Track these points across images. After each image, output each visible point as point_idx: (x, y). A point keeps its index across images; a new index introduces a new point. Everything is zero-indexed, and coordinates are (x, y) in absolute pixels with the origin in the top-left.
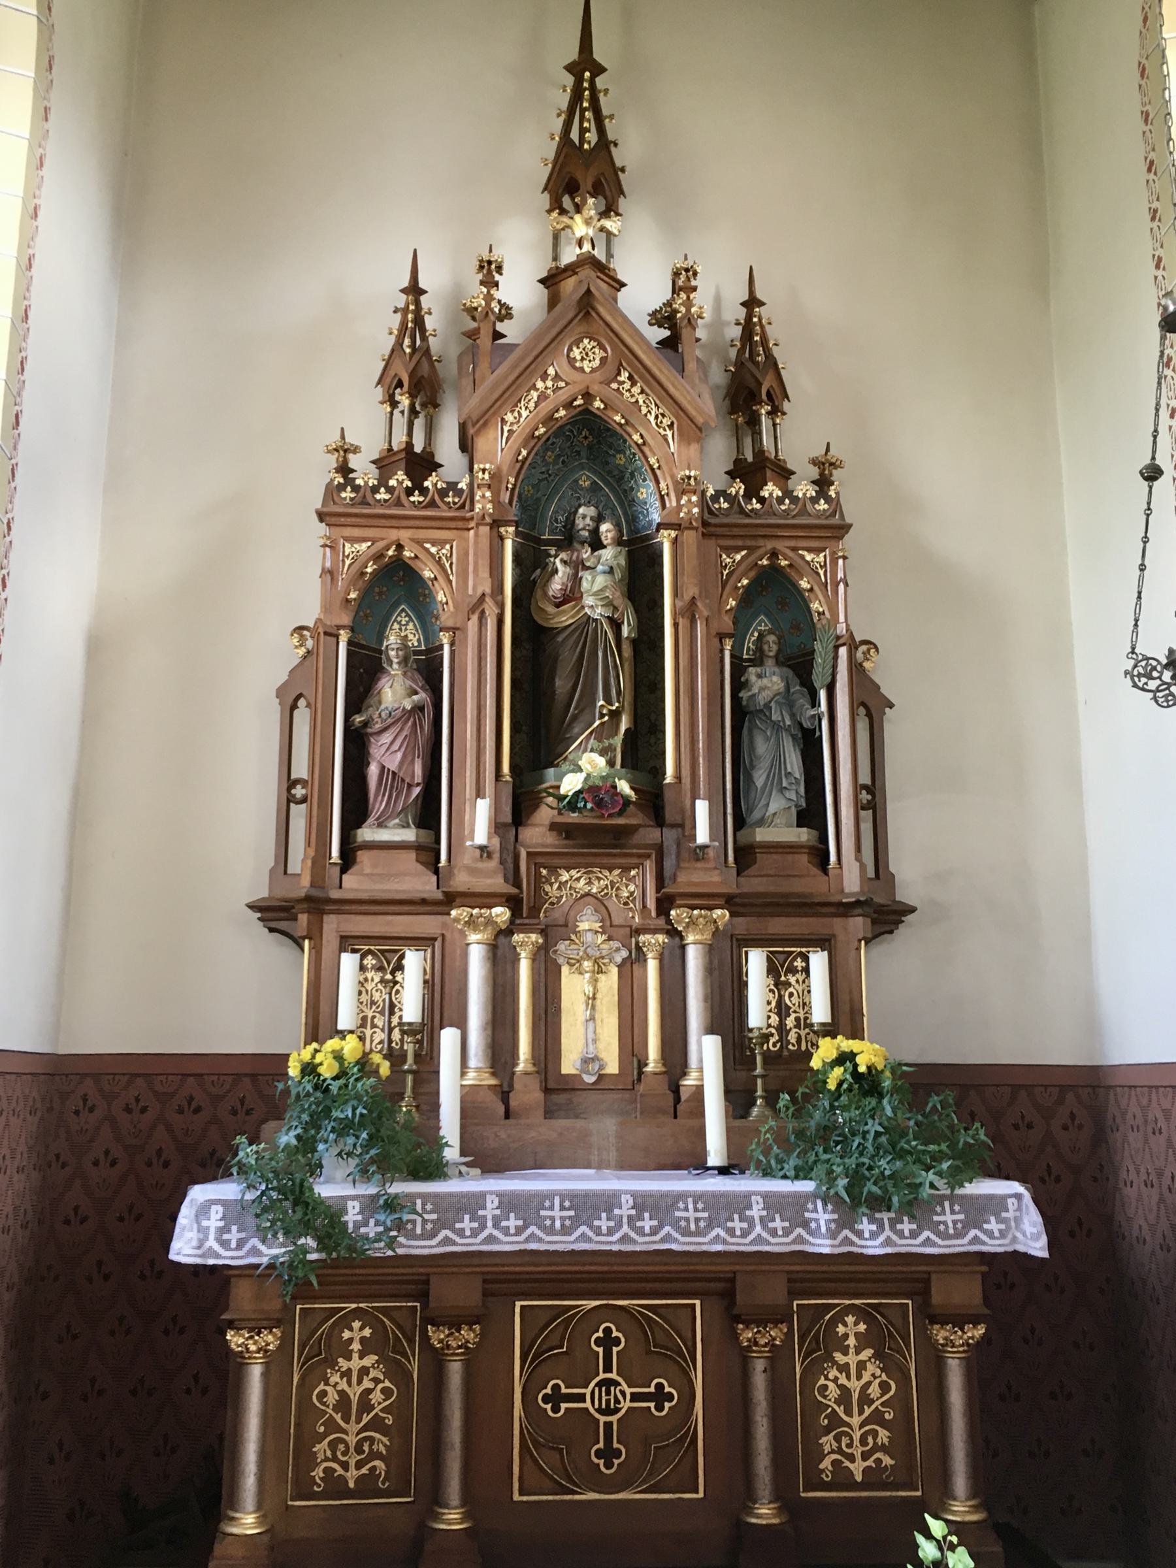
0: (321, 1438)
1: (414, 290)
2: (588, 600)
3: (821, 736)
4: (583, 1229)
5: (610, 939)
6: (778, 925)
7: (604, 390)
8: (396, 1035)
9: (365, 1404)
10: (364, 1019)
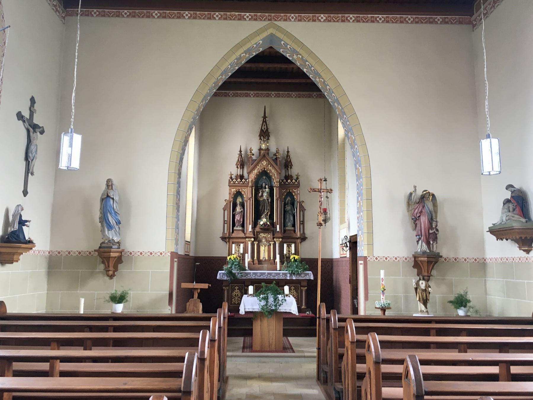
1: (241, 151)
9: (238, 295)
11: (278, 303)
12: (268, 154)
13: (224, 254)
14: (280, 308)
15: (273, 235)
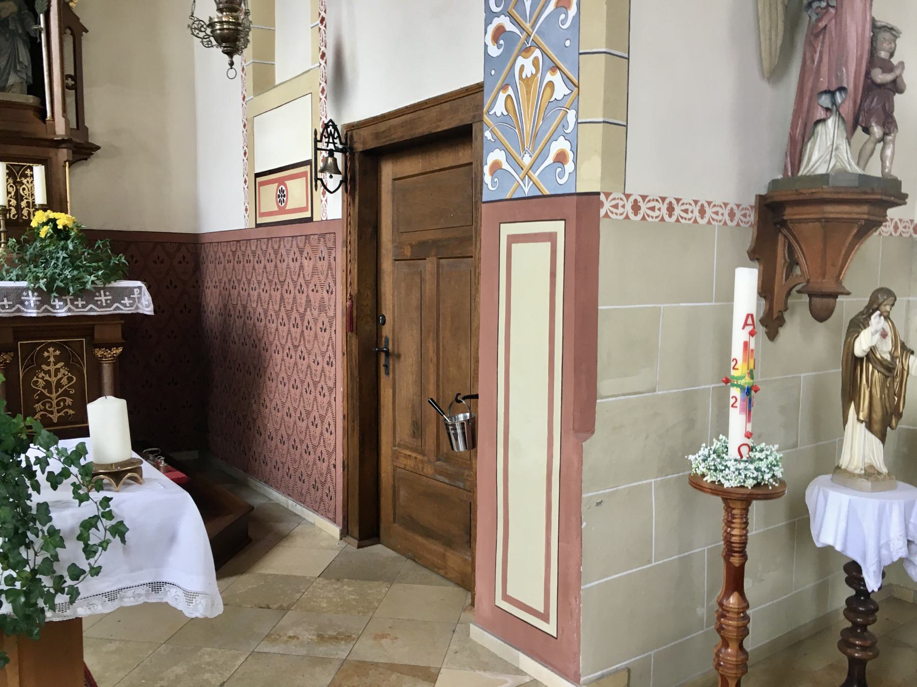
3: (41, 43)
6: (14, 150)
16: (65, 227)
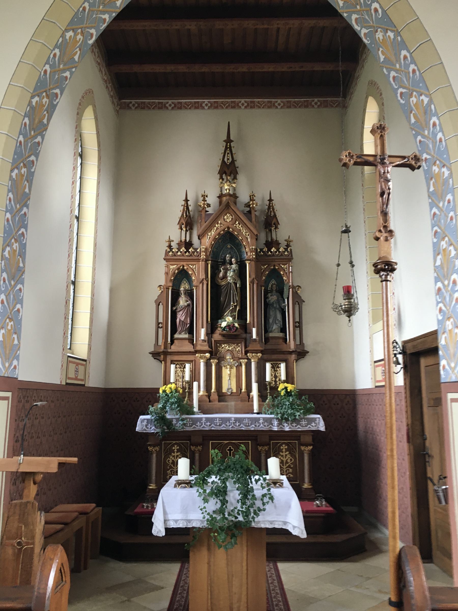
0: (168, 470)
1: (186, 200)
2: (229, 278)
4: (224, 425)
5: (234, 360)
6: (274, 357)
7: (232, 226)
8: (184, 383)
10: (177, 380)
11: (252, 505)
12: (235, 203)
13: (146, 382)
14: (259, 518)
15: (246, 347)
16: (291, 390)
